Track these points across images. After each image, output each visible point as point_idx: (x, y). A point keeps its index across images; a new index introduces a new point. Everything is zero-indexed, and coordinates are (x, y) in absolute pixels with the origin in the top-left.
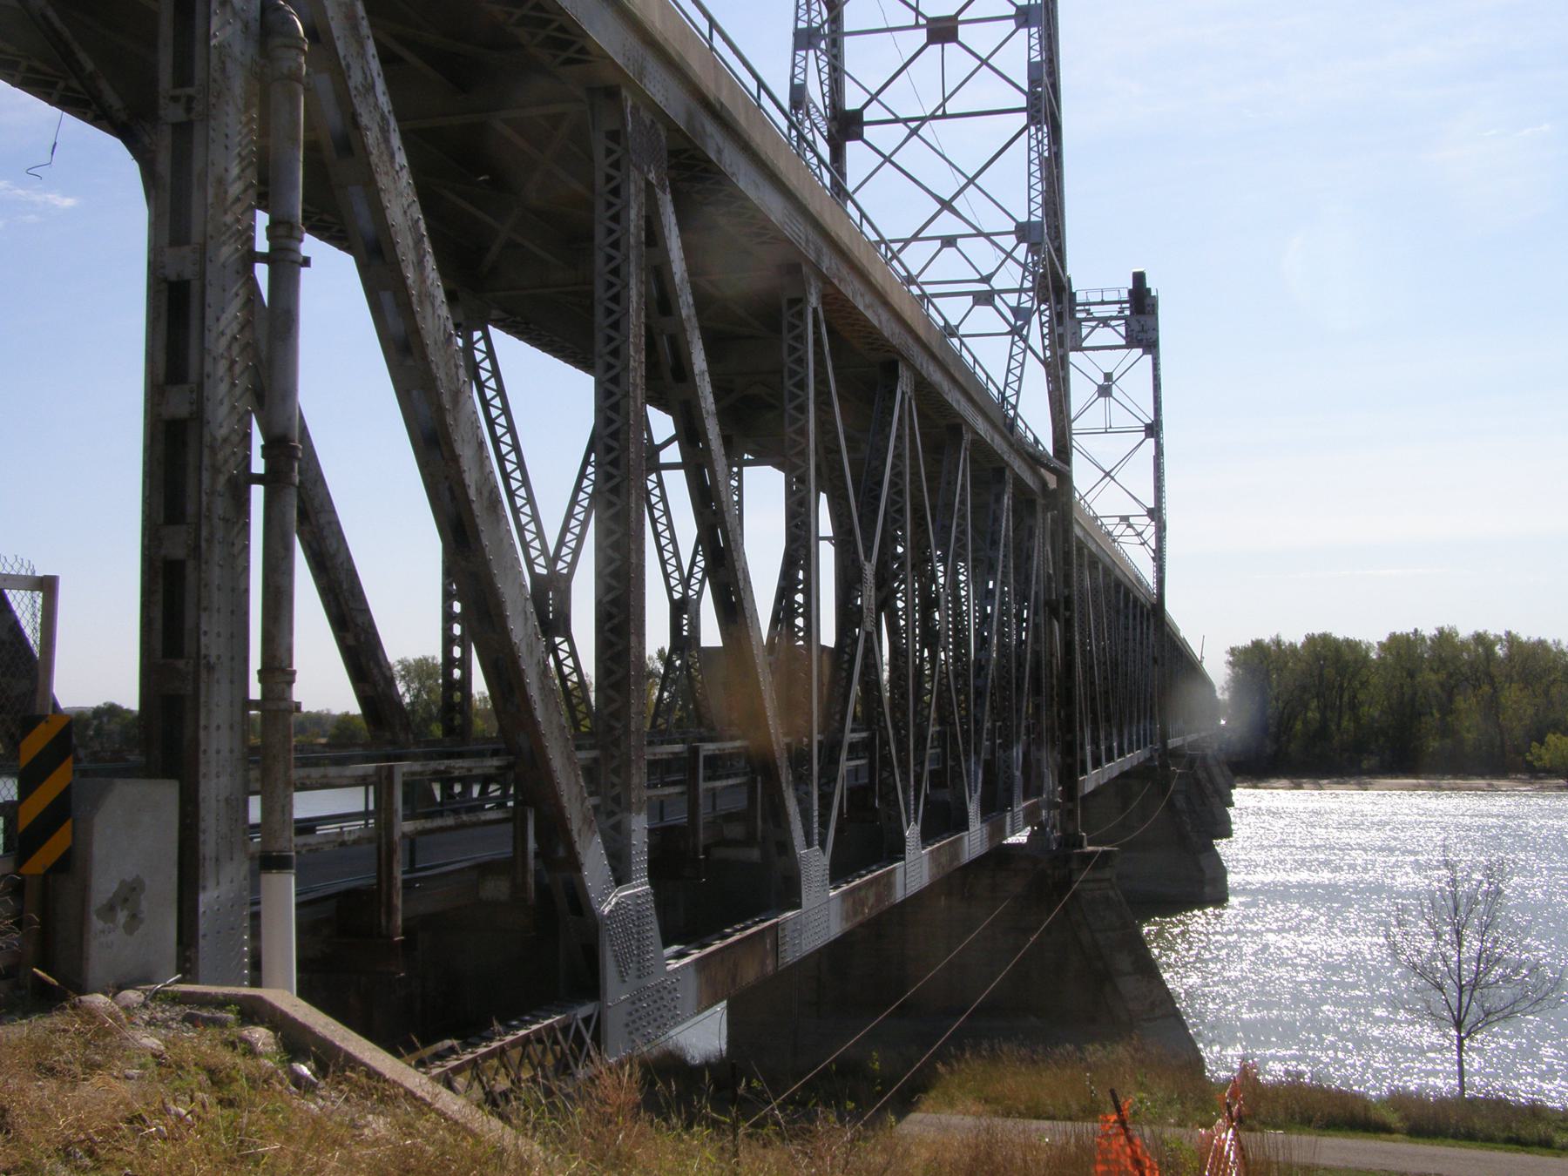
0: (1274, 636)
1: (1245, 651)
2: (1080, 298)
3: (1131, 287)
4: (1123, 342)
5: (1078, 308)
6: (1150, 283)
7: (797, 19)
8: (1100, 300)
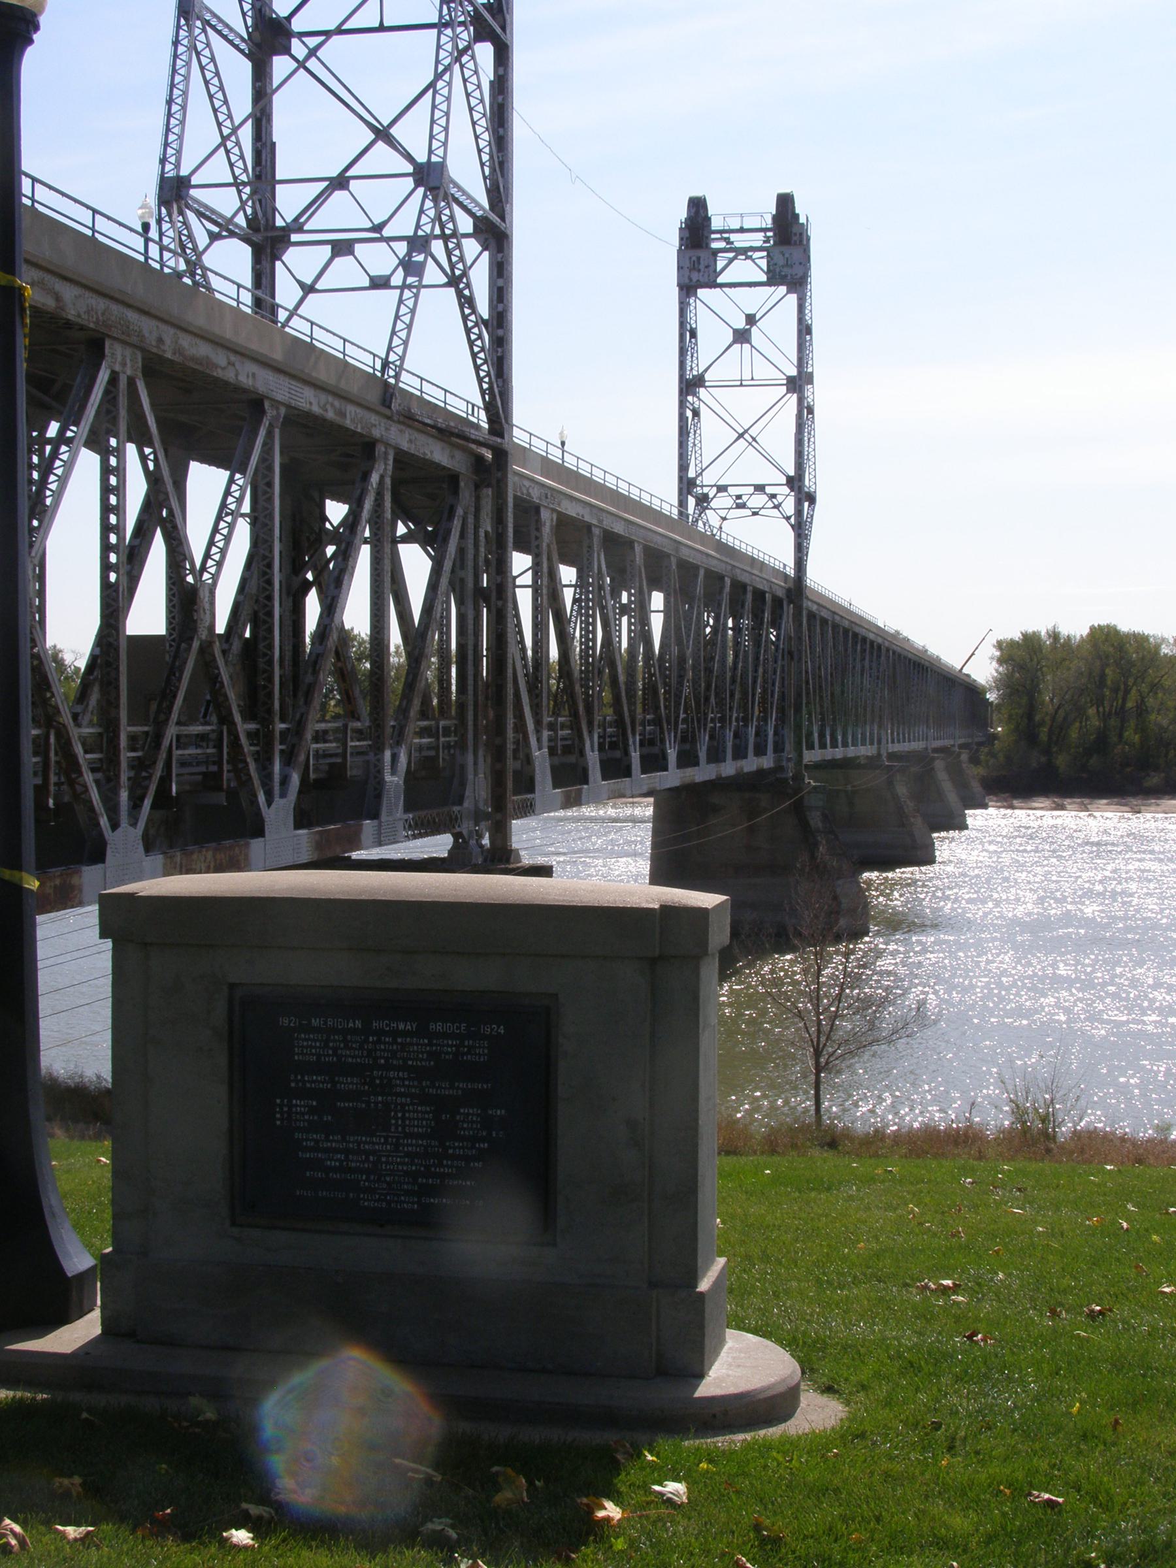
0: (1050, 627)
1: (1012, 644)
2: (716, 224)
3: (774, 212)
4: (764, 278)
5: (713, 236)
8: (738, 227)
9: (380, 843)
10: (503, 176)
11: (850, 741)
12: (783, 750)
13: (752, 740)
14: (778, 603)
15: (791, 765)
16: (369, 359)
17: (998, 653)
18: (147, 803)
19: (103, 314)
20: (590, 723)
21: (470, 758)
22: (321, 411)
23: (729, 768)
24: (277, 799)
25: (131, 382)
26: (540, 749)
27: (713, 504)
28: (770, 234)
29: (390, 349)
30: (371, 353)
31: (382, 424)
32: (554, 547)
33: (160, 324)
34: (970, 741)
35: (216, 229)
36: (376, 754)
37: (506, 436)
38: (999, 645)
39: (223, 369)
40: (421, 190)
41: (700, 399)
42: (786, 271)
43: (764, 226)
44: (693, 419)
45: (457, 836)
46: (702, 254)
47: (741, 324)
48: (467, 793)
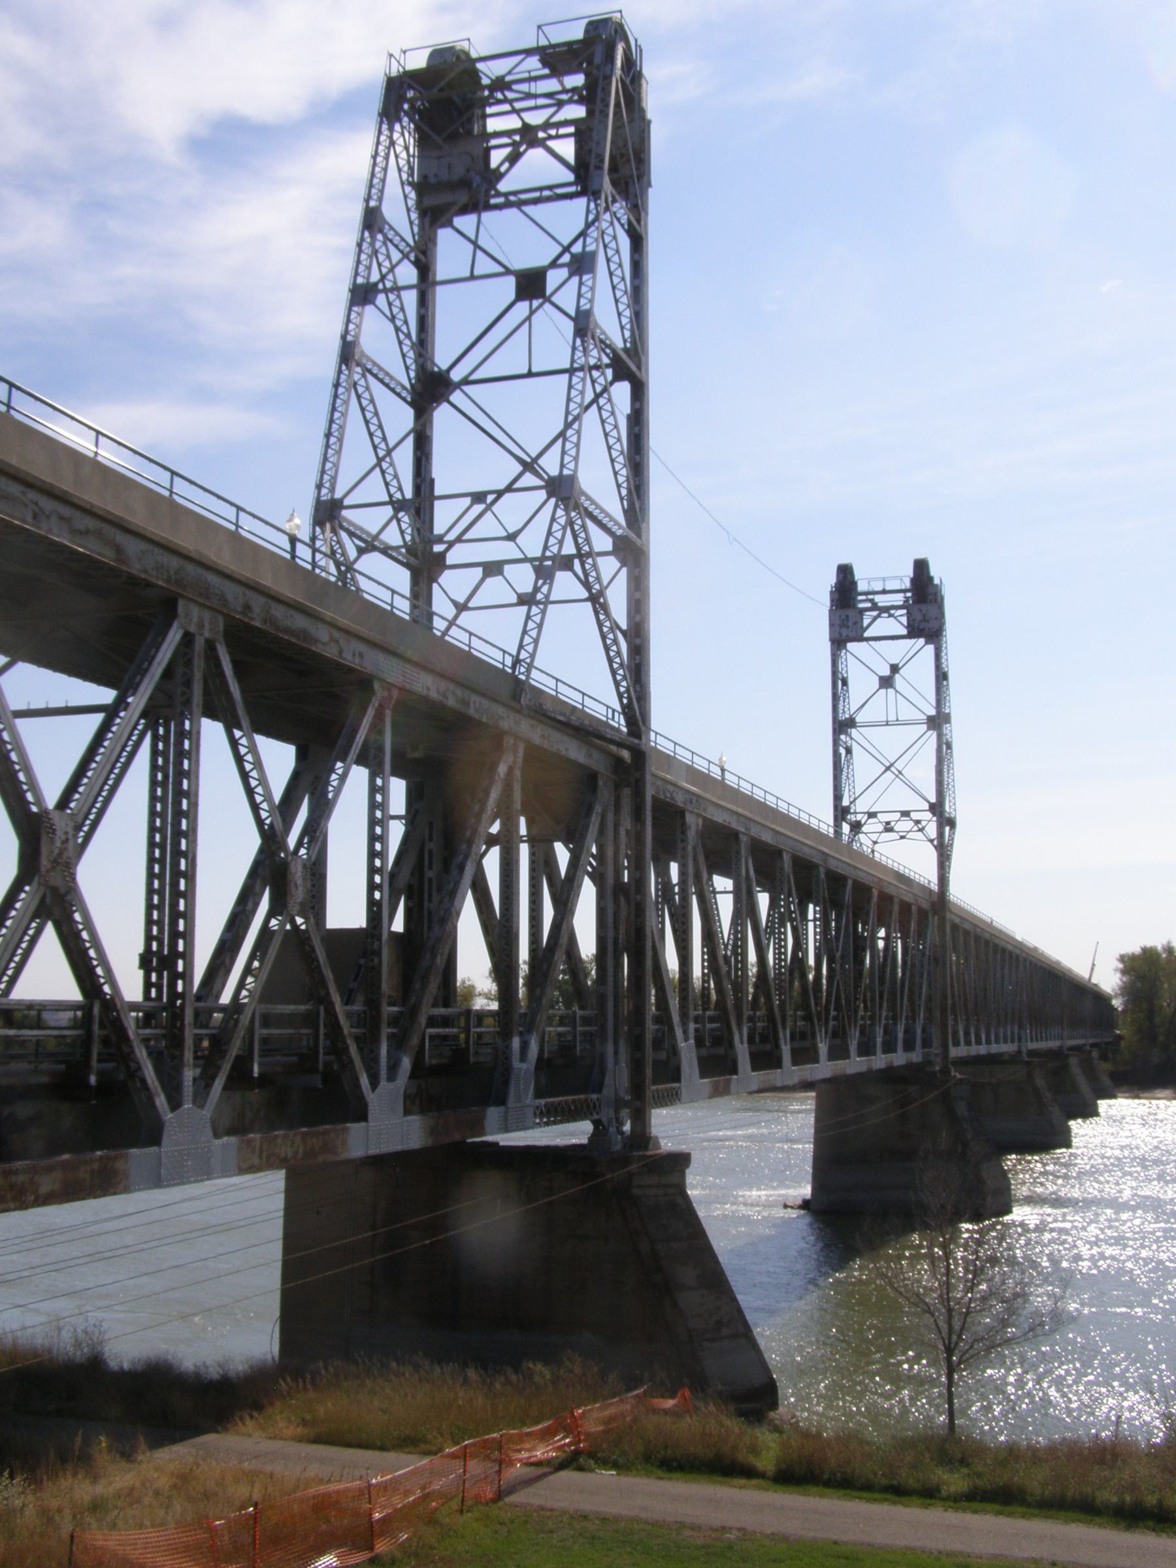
0: (1165, 942)
2: (862, 587)
3: (912, 575)
5: (860, 598)
6: (935, 572)
7: (357, 274)
8: (880, 589)
9: (506, 1129)
10: (639, 497)
11: (993, 1038)
12: (930, 1046)
13: (901, 1035)
14: (923, 914)
15: (938, 1060)
16: (498, 655)
17: (1121, 966)
18: (219, 1084)
19: (176, 573)
20: (739, 1017)
21: (610, 1049)
22: (441, 698)
23: (879, 1061)
24: (383, 1083)
25: (210, 646)
26: (686, 1040)
27: (864, 829)
28: (909, 594)
29: (521, 647)
30: (500, 649)
31: (511, 718)
32: (700, 850)
33: (247, 592)
34: (1099, 1040)
35: (363, 545)
36: (504, 1041)
37: (644, 738)
38: (1122, 958)
39: (325, 644)
40: (553, 501)
41: (852, 738)
42: (923, 625)
43: (903, 587)
44: (846, 756)
45: (596, 1123)
46: (850, 613)
47: (886, 672)
48: (606, 1082)
